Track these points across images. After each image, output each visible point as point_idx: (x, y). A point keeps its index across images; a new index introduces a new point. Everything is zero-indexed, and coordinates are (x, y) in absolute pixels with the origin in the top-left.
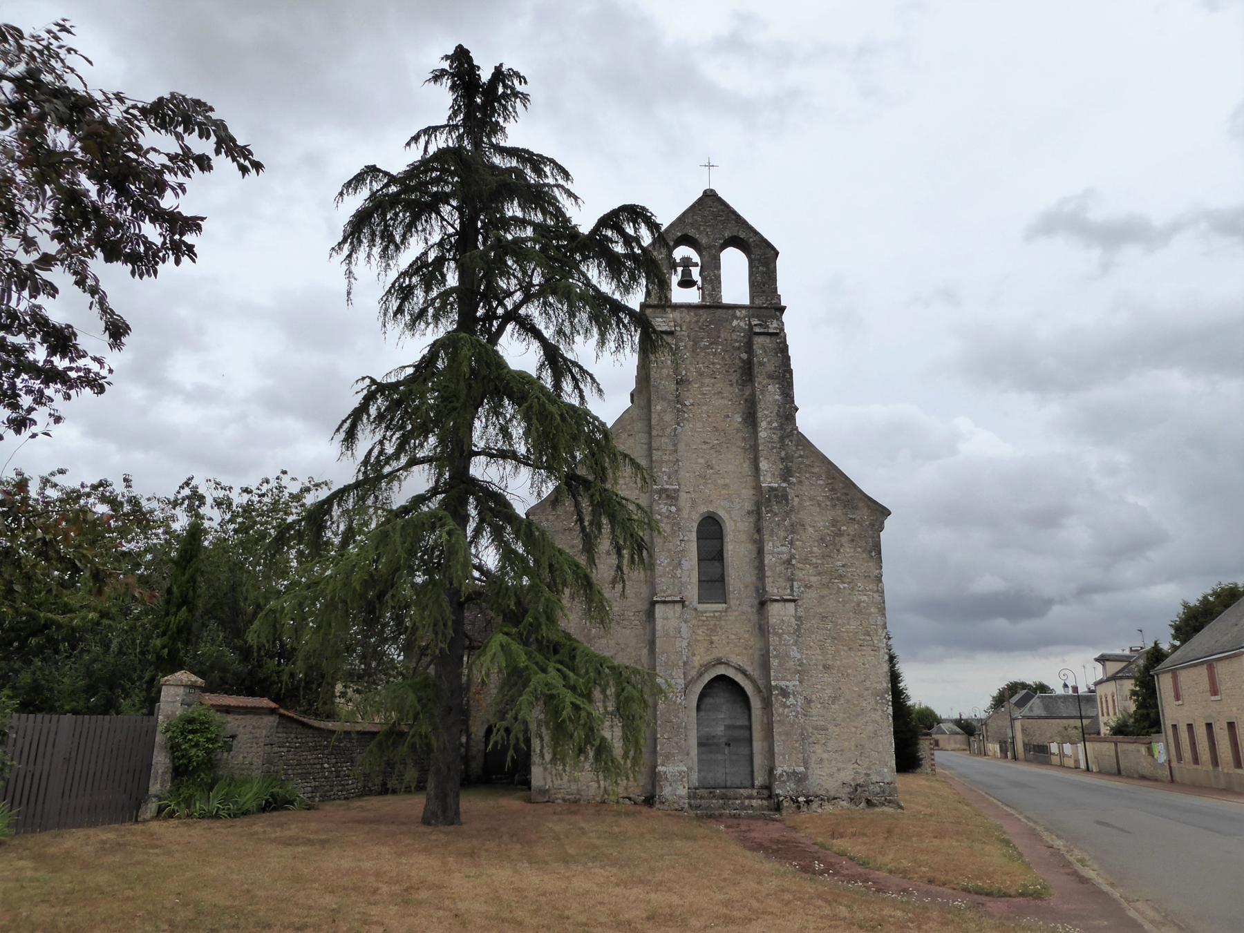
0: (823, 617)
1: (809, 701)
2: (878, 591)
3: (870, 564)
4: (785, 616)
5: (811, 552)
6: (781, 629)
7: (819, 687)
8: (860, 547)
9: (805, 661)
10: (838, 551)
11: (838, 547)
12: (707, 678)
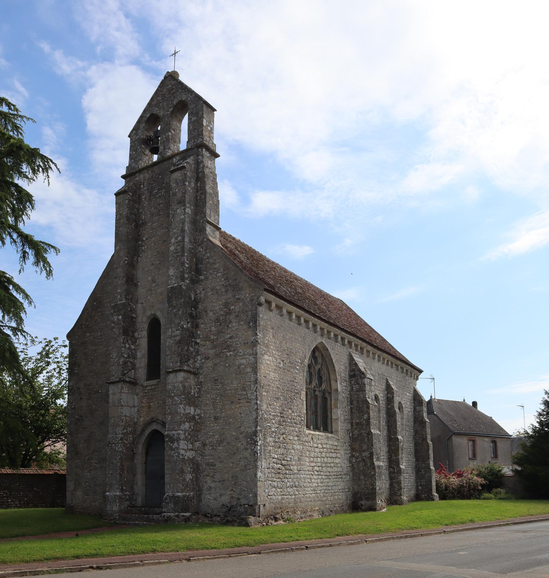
0: (215, 380)
1: (204, 445)
2: (253, 354)
3: (249, 333)
4: (176, 383)
5: (210, 331)
6: (173, 393)
7: (211, 434)
8: (242, 320)
9: (202, 415)
10: (228, 326)
11: (228, 324)
12: (147, 432)
